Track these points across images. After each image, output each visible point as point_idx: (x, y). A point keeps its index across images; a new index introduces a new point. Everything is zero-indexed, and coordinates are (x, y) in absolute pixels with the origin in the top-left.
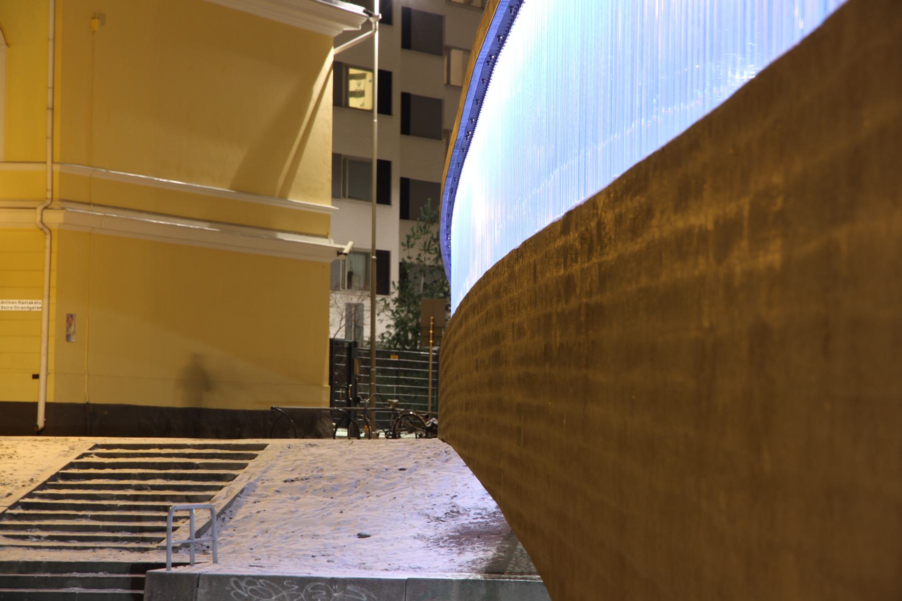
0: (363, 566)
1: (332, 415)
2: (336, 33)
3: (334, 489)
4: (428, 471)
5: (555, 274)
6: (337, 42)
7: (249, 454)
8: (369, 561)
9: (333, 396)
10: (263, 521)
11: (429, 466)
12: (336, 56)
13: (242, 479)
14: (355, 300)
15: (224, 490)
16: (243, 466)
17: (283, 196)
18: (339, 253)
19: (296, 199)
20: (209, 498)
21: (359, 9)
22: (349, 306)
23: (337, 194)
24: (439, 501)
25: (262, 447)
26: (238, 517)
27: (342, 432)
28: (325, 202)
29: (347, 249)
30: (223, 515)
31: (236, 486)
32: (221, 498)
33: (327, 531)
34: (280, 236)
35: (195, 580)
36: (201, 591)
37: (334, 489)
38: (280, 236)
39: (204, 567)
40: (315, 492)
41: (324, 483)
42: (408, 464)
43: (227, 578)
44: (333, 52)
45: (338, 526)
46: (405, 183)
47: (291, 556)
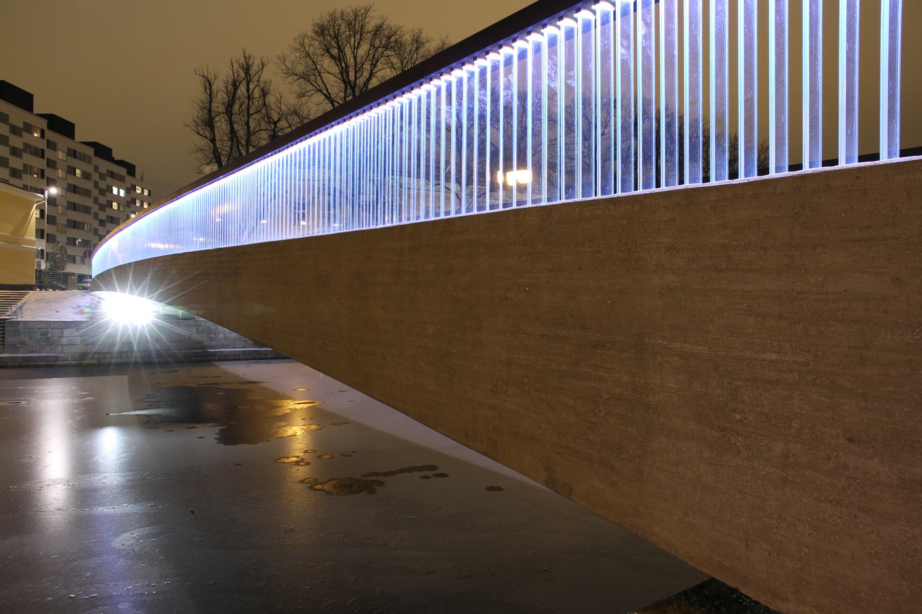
0: (59, 318)
1: (36, 286)
2: (36, 201)
3: (48, 302)
4: (71, 298)
5: (146, 246)
6: (37, 203)
7: (25, 294)
8: (60, 317)
9: (36, 281)
10: (187, 322)
11: (71, 297)
12: (36, 206)
13: (24, 300)
14: (39, 260)
15: (19, 303)
16: (24, 297)
17: (23, 237)
18: (38, 249)
19: (26, 237)
20: (16, 304)
21: (42, 196)
22: (709, 181)
23: (37, 237)
24: (75, 304)
25: (28, 293)
26: (24, 308)
27: (38, 290)
28: (34, 239)
29: (40, 249)
30: (20, 308)
31: (23, 301)
32: (19, 304)
33: (48, 311)
34: (23, 245)
35: (19, 322)
36: (21, 325)
37: (48, 302)
38: (23, 245)
39: (19, 319)
40: (43, 303)
41: (45, 301)
42: (66, 296)
43: (27, 322)
44: (35, 205)
45: (51, 310)
46: (47, 234)
47: (40, 316)
